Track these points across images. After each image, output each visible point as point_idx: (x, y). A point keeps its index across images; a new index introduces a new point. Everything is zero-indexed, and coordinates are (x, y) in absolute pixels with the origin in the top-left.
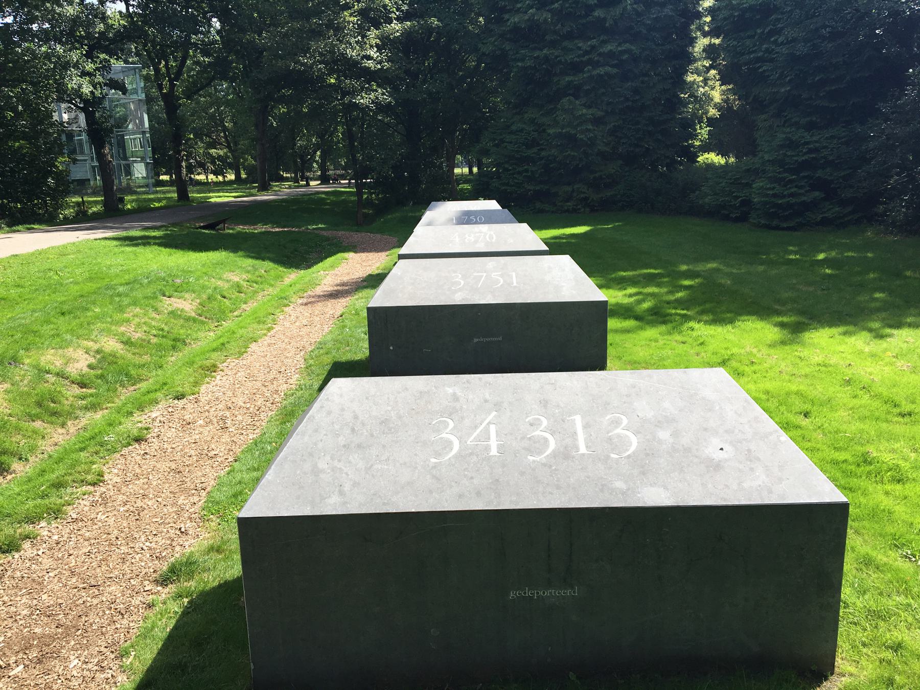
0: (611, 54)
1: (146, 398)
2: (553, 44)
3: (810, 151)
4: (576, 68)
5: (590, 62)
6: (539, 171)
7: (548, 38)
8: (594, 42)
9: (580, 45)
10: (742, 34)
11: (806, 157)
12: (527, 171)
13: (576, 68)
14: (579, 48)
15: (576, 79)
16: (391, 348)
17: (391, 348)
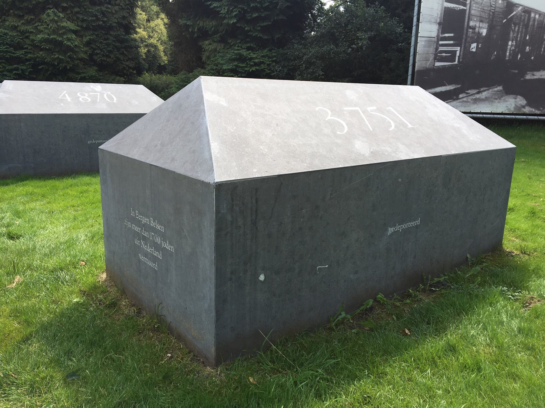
6: (29, 70)
12: (17, 69)
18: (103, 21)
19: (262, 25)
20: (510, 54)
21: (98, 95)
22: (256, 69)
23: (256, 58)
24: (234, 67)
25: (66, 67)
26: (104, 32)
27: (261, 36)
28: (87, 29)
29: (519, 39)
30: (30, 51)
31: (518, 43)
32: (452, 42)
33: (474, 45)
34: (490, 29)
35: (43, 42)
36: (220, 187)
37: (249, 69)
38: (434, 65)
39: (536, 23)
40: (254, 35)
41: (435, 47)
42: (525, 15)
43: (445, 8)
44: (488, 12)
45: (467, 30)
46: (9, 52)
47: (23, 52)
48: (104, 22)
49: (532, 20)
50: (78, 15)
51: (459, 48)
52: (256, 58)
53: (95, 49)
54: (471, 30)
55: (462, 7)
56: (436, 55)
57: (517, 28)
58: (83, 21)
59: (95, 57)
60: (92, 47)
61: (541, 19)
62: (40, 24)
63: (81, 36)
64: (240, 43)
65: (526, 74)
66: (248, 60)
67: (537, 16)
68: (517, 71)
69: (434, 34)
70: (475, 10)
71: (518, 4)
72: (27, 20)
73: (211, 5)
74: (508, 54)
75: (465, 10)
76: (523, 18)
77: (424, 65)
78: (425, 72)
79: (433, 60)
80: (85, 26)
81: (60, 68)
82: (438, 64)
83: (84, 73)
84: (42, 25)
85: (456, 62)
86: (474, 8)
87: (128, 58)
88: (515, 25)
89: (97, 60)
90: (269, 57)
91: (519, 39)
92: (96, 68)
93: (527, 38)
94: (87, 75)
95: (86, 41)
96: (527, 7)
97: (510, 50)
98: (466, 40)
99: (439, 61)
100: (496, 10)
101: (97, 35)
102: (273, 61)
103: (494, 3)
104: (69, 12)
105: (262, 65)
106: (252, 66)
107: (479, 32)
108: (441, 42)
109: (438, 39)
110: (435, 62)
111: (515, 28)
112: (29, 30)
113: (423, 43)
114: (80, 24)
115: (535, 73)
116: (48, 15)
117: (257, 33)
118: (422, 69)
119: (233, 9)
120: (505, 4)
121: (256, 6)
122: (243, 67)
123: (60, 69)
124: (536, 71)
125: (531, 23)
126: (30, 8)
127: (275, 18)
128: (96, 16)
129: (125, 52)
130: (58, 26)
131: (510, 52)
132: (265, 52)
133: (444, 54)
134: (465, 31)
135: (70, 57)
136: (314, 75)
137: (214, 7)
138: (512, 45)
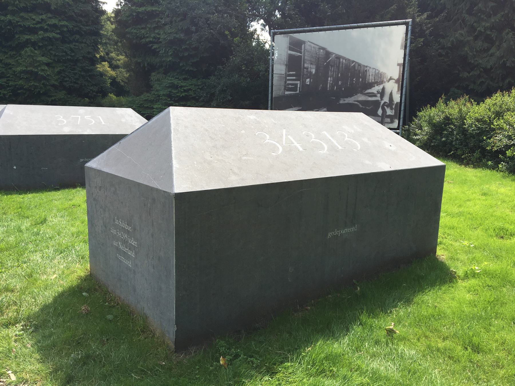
0: (55, 26)
1: (38, 26)
2: (13, 13)
3: (185, 91)
4: (33, 31)
5: (42, 29)
6: (9, 94)
7: (10, 8)
8: (44, 17)
9: (34, 17)
10: (139, 26)
11: (183, 94)
13: (33, 31)
14: (34, 20)
15: (33, 38)
16: (15, 167)
17: (15, 167)
18: (71, 56)
19: (193, 61)
20: (330, 86)
21: (79, 117)
22: (185, 95)
23: (185, 86)
25: (39, 92)
26: (72, 64)
27: (192, 69)
29: (334, 76)
30: (12, 79)
31: (334, 79)
32: (294, 78)
33: (308, 80)
34: (317, 70)
36: (181, 197)
37: (180, 94)
38: (284, 93)
39: (344, 66)
40: (186, 69)
41: (284, 81)
42: (337, 60)
43: (289, 54)
44: (315, 57)
45: (303, 70)
47: (5, 80)
49: (341, 63)
50: (52, 52)
51: (299, 82)
53: (64, 77)
54: (305, 70)
55: (299, 54)
56: (285, 87)
57: (333, 69)
58: (55, 55)
59: (65, 84)
61: (347, 63)
62: (20, 58)
63: (54, 67)
64: (177, 75)
65: (340, 100)
66: (179, 87)
67: (344, 61)
68: (334, 98)
69: (283, 72)
70: (307, 56)
71: (333, 53)
72: (10, 55)
73: (152, 46)
74: (328, 86)
75: (301, 56)
76: (336, 62)
77: (278, 94)
78: (279, 98)
79: (284, 90)
81: (35, 92)
82: (287, 93)
83: (55, 96)
84: (22, 59)
85: (298, 92)
86: (307, 55)
88: (332, 66)
90: (195, 85)
91: (334, 76)
92: (64, 92)
93: (339, 76)
95: (58, 71)
96: (338, 55)
97: (330, 84)
98: (303, 76)
99: (287, 91)
100: (320, 56)
101: (66, 67)
103: (318, 52)
104: (44, 49)
105: (190, 91)
106: (182, 92)
107: (310, 71)
108: (288, 78)
109: (286, 75)
110: (285, 91)
111: (331, 69)
112: (11, 63)
113: (277, 78)
114: (52, 58)
115: (345, 99)
118: (277, 96)
120: (325, 53)
123: (36, 93)
124: (346, 98)
125: (341, 65)
126: (102, 23)
127: (201, 56)
128: (66, 52)
129: (89, 79)
130: (33, 59)
131: (330, 85)
132: (194, 81)
133: (290, 86)
134: (302, 71)
135: (43, 84)
136: (225, 100)
137: (155, 48)
138: (331, 80)
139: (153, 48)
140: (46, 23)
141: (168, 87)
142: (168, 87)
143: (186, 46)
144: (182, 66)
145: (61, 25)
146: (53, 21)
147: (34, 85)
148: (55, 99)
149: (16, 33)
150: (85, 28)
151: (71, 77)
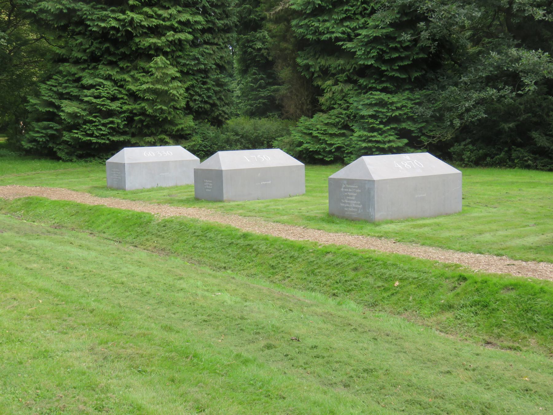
0: (187, 24)
8: (173, 11)
12: (112, 122)
13: (156, 31)
23: (397, 102)
24: (374, 113)
28: (187, 73)
35: (148, 92)
46: (105, 105)
48: (205, 64)
52: (397, 102)
53: (192, 96)
58: (185, 65)
60: (190, 94)
66: (389, 104)
80: (185, 70)
87: (225, 103)
89: (193, 107)
92: (192, 117)
94: (185, 126)
101: (197, 80)
102: (415, 104)
106: (393, 110)
116: (156, 63)
117: (394, 73)
119: (371, 50)
121: (396, 46)
122: (384, 112)
123: (160, 120)
128: (197, 59)
139: (344, 47)
140: (176, 20)
141: (376, 105)
142: (376, 105)
143: (396, 45)
144: (89, 19)
145: (196, 22)
146: (184, 17)
147: (161, 109)
148: (182, 128)
149: (136, 36)
150: (220, 23)
151: (203, 94)
